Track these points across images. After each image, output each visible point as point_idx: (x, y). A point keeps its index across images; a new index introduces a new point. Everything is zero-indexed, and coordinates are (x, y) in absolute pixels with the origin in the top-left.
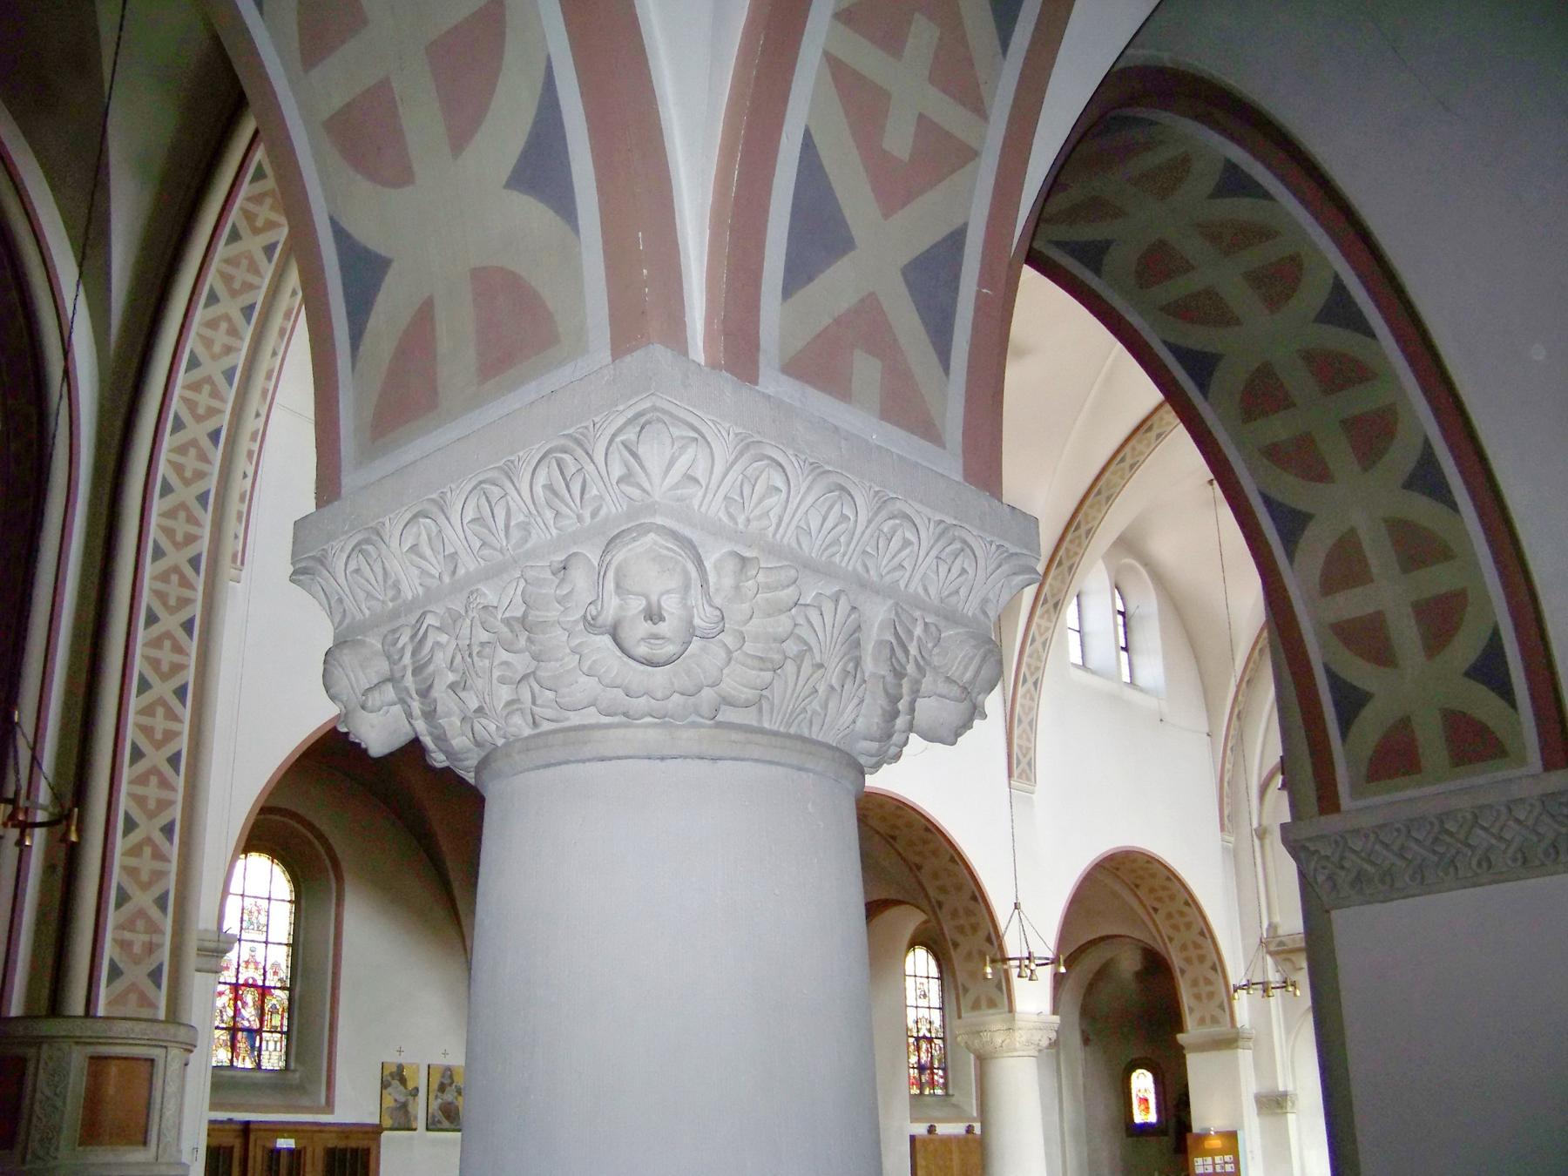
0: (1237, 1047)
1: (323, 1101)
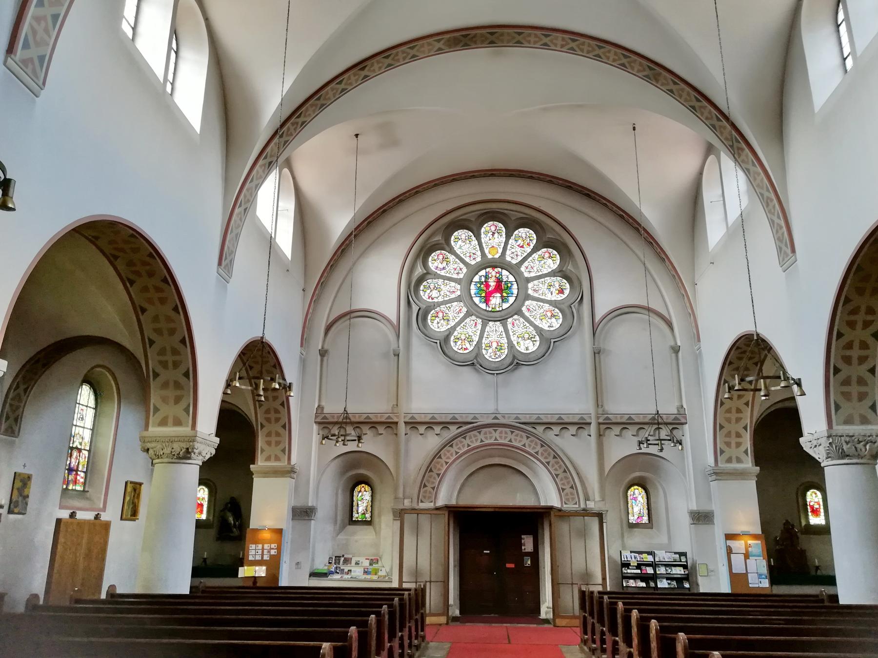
1: (101, 506)
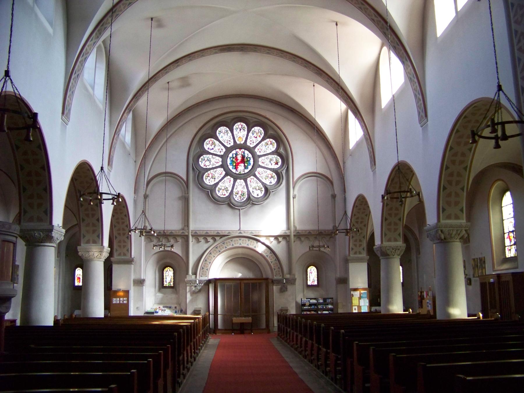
0: (132, 264)
